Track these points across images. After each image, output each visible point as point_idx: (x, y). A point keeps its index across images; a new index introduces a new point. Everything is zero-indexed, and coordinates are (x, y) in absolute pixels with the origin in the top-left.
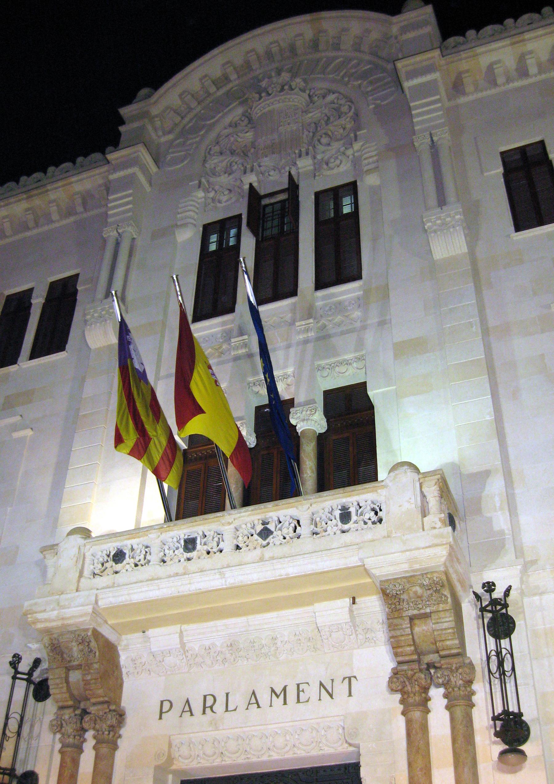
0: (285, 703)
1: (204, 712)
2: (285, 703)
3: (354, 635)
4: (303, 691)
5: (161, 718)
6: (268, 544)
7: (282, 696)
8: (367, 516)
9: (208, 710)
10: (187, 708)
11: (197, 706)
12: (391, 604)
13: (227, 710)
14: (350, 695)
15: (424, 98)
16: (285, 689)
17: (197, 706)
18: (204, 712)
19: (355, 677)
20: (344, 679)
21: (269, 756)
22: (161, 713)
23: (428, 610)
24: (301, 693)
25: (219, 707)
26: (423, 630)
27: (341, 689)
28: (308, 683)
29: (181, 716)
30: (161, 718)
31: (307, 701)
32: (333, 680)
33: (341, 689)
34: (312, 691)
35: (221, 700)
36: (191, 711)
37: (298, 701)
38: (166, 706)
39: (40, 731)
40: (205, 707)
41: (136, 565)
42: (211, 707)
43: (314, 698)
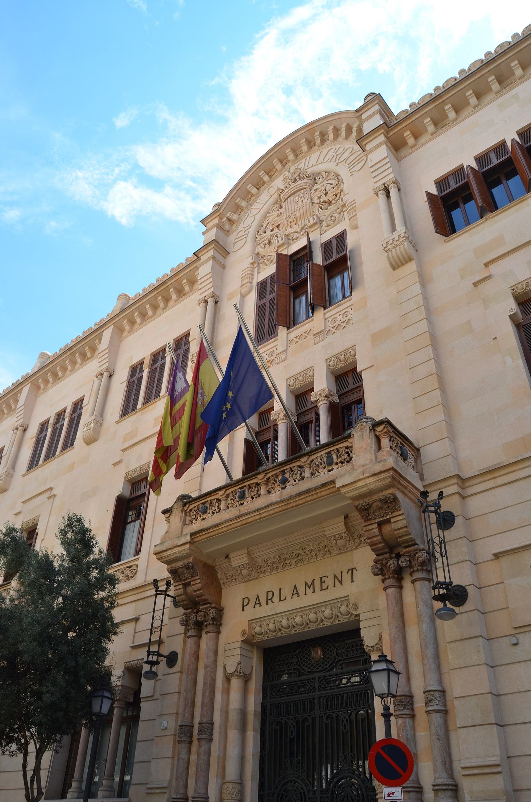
0: (314, 592)
1: (267, 604)
2: (314, 592)
3: (352, 540)
4: (324, 582)
5: (243, 610)
6: (286, 487)
7: (312, 587)
8: (343, 458)
9: (270, 601)
10: (295, 592)
11: (263, 600)
12: (363, 516)
13: (280, 600)
14: (353, 581)
15: (529, 168)
16: (313, 582)
17: (263, 600)
18: (267, 604)
19: (355, 568)
20: (349, 570)
21: (339, 621)
22: (243, 606)
23: (388, 517)
24: (323, 584)
25: (276, 599)
26: (388, 530)
27: (347, 577)
28: (327, 576)
29: (254, 607)
30: (243, 610)
31: (327, 588)
32: (342, 572)
33: (347, 577)
34: (329, 582)
35: (277, 593)
36: (298, 593)
37: (322, 589)
38: (246, 601)
39: (134, 637)
40: (268, 600)
41: (213, 513)
42: (271, 599)
43: (331, 585)
